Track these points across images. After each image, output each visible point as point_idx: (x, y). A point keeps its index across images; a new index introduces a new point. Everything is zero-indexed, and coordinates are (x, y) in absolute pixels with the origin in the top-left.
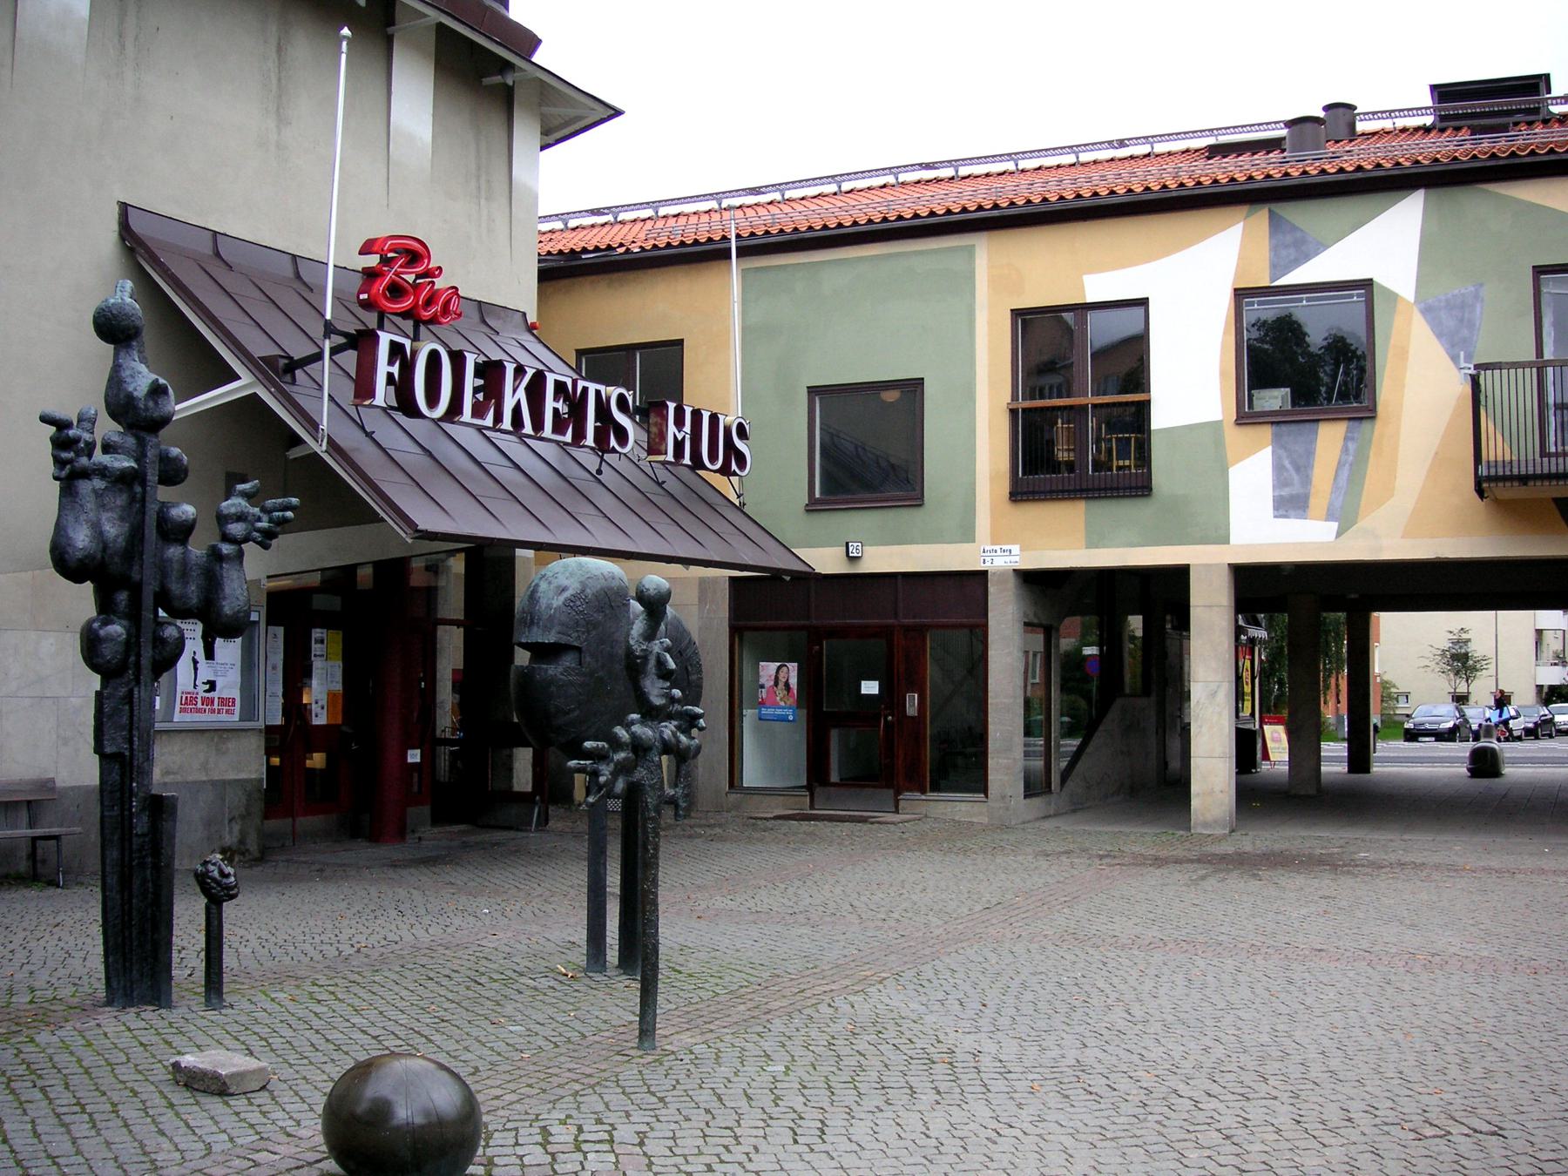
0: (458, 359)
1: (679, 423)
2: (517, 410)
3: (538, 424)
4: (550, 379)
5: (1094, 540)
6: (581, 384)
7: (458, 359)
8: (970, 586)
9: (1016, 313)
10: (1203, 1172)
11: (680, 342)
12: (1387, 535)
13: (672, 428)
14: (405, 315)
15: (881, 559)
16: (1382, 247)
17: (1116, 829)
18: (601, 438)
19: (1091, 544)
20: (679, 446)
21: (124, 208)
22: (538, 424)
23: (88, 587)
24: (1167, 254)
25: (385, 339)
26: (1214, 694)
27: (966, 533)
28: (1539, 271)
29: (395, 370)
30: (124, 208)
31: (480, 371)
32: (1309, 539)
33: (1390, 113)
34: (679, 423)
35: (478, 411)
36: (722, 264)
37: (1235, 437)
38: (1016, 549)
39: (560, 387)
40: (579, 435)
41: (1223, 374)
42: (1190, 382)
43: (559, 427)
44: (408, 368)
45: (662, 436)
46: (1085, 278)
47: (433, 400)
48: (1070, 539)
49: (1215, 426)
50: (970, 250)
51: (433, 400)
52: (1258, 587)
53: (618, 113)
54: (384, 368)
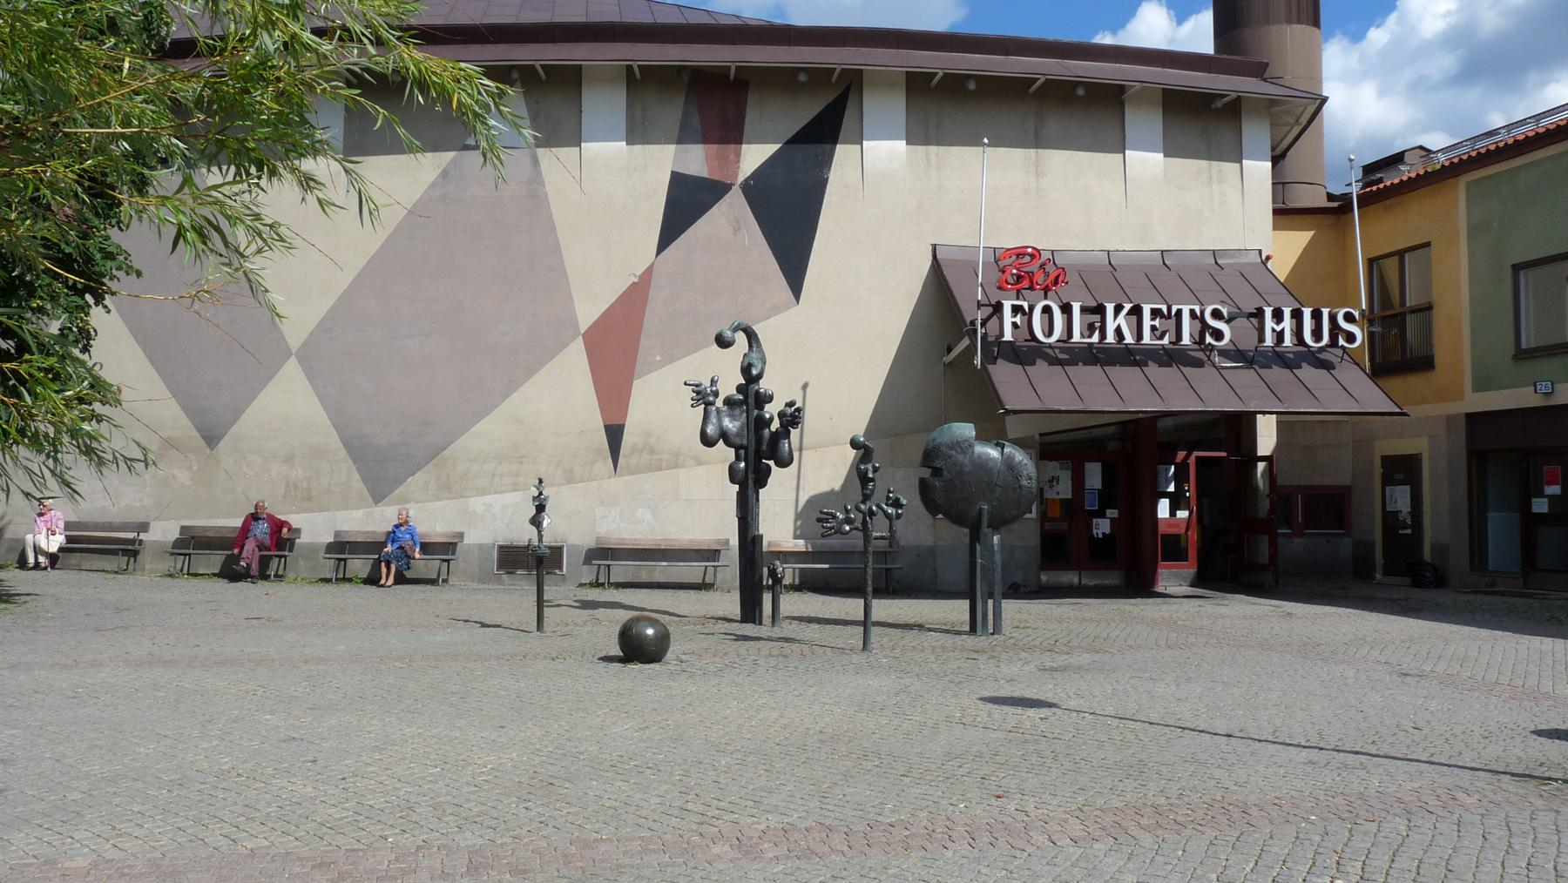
2: (1118, 331)
3: (1140, 336)
7: (1066, 309)
13: (1269, 323)
20: (1280, 336)
21: (934, 247)
25: (1007, 306)
39: (1156, 313)
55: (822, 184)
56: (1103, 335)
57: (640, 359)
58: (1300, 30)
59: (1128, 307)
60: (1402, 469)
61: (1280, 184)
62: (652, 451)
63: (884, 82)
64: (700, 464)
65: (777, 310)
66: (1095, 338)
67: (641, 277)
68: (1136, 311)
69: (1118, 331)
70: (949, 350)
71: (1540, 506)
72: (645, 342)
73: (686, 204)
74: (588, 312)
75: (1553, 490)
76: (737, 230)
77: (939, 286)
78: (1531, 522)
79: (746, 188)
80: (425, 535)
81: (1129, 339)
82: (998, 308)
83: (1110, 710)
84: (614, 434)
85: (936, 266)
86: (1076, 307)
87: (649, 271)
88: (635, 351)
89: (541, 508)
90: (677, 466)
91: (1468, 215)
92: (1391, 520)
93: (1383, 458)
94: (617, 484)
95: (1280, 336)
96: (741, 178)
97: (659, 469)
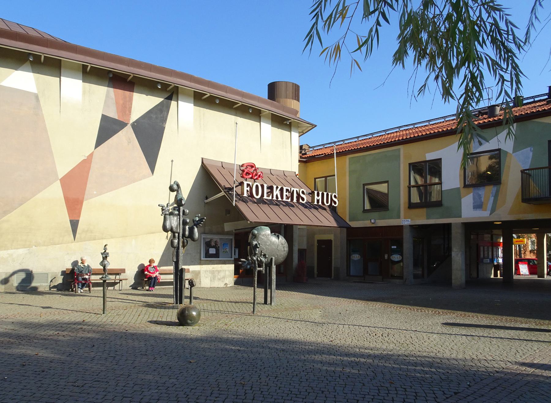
0: (262, 186)
1: (318, 195)
2: (277, 196)
3: (282, 198)
4: (285, 189)
5: (428, 218)
6: (292, 189)
7: (262, 186)
8: (400, 228)
9: (410, 164)
11: (441, 159)
12: (504, 213)
13: (316, 197)
14: (251, 178)
15: (382, 223)
16: (502, 141)
19: (428, 218)
20: (318, 201)
21: (203, 159)
22: (282, 198)
24: (443, 148)
25: (245, 183)
26: (457, 255)
27: (399, 217)
28: (315, 179)
29: (248, 189)
30: (203, 159)
31: (268, 188)
32: (482, 215)
33: (407, 126)
34: (318, 195)
36: (329, 161)
37: (463, 191)
38: (410, 220)
39: (287, 190)
40: (292, 199)
41: (460, 175)
42: (451, 177)
43: (288, 198)
46: (426, 154)
47: (257, 194)
48: (421, 218)
49: (458, 189)
50: (399, 150)
51: (257, 194)
52: (471, 228)
53: (316, 126)
54: (246, 188)
55: (164, 128)
56: (273, 197)
57: (87, 192)
59: (280, 187)
61: (465, 150)
65: (144, 177)
66: (270, 198)
67: (88, 157)
68: (282, 190)
69: (277, 196)
70: (207, 198)
72: (89, 185)
73: (108, 129)
74: (63, 170)
77: (523, 172)
79: (133, 125)
80: (94, 269)
81: (280, 199)
82: (241, 184)
83: (404, 328)
84: (74, 225)
86: (265, 186)
87: (91, 155)
88: (85, 189)
89: (105, 258)
91: (349, 168)
93: (318, 241)
95: (318, 201)
96: (131, 122)
97: (95, 239)
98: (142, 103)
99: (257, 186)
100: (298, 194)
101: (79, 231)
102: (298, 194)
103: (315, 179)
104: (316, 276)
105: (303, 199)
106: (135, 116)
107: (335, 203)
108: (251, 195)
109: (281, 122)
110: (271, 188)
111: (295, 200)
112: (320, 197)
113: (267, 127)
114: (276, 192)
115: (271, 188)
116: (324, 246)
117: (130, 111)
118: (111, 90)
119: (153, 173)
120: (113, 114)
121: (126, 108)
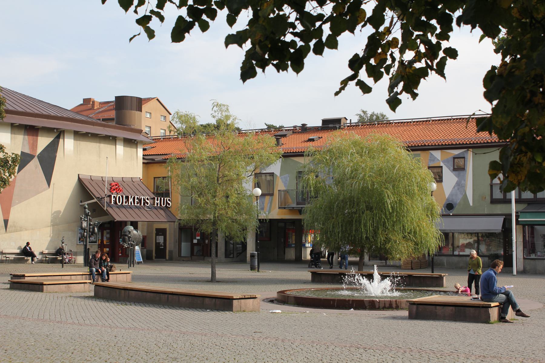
0: (122, 197)
1: (157, 200)
3: (134, 203)
4: (136, 197)
7: (122, 197)
10: (365, 1)
13: (156, 201)
17: (192, 275)
18: (144, 204)
20: (157, 204)
22: (134, 203)
23: (251, 46)
25: (113, 196)
28: (154, 178)
34: (157, 200)
35: (126, 203)
36: (508, 205)
39: (137, 198)
40: (141, 204)
43: (138, 203)
44: (116, 199)
45: (155, 202)
47: (119, 202)
51: (119, 202)
54: (113, 199)
55: (56, 156)
57: (13, 202)
58: (138, 113)
60: (161, 232)
62: (15, 227)
63: (69, 131)
64: (26, 230)
65: (44, 190)
68: (134, 198)
70: (81, 202)
71: (195, 241)
75: (199, 238)
76: (36, 168)
78: (193, 245)
84: (6, 222)
85: (80, 180)
86: (124, 196)
88: (12, 198)
90: (21, 231)
92: (158, 245)
93: (157, 229)
94: (7, 235)
96: (37, 154)
98: (43, 142)
99: (119, 197)
100: (144, 200)
101: (8, 227)
102: (144, 200)
103: (154, 178)
104: (154, 258)
105: (147, 203)
106: (40, 149)
107: (169, 204)
108: (115, 202)
109: (130, 142)
110: (127, 198)
111: (142, 205)
112: (159, 201)
113: (120, 148)
114: (131, 200)
115: (127, 198)
116: (440, 7)
117: (36, 148)
118: (26, 137)
119: (49, 187)
120: (27, 151)
121: (34, 146)
